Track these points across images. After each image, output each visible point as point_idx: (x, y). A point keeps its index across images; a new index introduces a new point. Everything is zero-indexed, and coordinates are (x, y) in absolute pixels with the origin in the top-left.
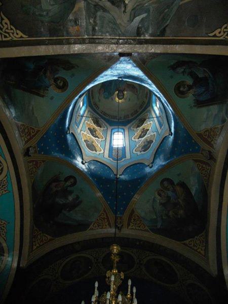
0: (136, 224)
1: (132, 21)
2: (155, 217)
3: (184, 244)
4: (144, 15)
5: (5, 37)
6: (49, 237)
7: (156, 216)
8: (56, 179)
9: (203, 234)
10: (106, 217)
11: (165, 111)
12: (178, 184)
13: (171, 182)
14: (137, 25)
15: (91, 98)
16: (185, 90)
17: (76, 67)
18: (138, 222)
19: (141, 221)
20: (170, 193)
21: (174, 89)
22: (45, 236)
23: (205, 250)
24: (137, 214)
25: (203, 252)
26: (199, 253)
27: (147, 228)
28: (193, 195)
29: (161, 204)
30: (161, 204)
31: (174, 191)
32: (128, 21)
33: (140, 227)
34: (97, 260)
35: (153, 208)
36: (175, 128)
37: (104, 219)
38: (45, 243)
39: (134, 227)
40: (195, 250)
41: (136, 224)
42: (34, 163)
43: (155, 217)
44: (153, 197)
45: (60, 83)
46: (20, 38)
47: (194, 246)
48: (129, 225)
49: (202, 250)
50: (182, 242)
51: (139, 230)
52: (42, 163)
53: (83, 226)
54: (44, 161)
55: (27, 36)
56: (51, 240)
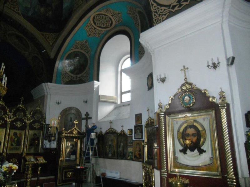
3: (43, 35)
4: (23, 115)
5: (155, 20)
7: (31, 6)
9: (57, 34)
11: (107, 102)
23: (53, 43)
25: (51, 44)
26: (49, 43)
27: (19, 12)
28: (64, 7)
33: (14, 8)
36: (219, 145)
39: (9, 6)
40: (47, 40)
41: (12, 5)
45: (54, 122)
46: (164, 11)
47: (48, 38)
55: (167, 8)
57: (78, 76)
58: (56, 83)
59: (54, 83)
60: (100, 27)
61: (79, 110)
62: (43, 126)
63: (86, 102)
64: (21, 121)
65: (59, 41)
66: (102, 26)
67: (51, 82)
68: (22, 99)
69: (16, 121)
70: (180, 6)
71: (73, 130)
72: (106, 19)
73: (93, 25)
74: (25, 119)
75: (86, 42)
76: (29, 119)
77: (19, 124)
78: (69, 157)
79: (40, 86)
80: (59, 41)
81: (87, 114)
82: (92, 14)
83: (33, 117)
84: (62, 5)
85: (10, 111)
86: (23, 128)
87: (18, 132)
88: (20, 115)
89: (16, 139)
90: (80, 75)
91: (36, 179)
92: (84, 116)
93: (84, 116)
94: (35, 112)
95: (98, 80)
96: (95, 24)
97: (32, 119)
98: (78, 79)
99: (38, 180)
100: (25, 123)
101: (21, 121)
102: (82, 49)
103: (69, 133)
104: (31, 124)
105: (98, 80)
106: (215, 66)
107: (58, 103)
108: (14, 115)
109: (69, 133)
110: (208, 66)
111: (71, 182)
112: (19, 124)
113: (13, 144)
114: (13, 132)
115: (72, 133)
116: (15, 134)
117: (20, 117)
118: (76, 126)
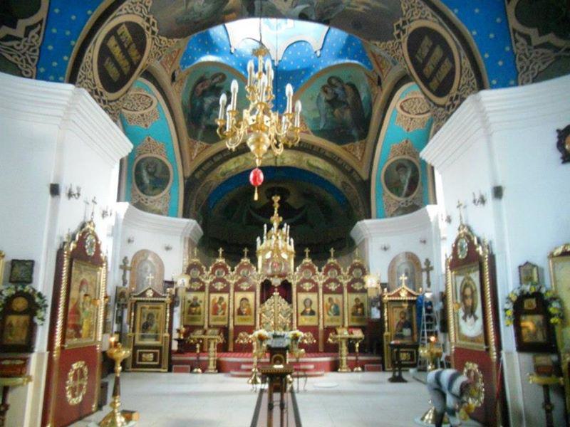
3: (346, 149)
26: (357, 158)
27: (308, 129)
50: (343, 146)
56: (207, 147)
57: (409, 199)
58: (377, 217)
59: (374, 219)
60: (420, 114)
61: (415, 255)
62: (115, 327)
63: (425, 242)
64: (336, 281)
65: (368, 152)
66: (421, 112)
67: (369, 216)
68: (332, 251)
69: (329, 281)
70: (454, 105)
71: (400, 290)
72: (415, 109)
73: (406, 114)
74: (340, 278)
75: (407, 142)
76: (345, 278)
77: (333, 287)
78: (401, 331)
79: (355, 227)
80: (368, 152)
81: (428, 262)
82: (396, 103)
83: (350, 273)
84: (359, 97)
85: (320, 270)
86: (340, 291)
87: (334, 297)
88: (332, 274)
89: (332, 307)
90: (413, 196)
91: (353, 358)
92: (424, 266)
93: (424, 266)
94: (354, 267)
95: (435, 202)
96: (408, 112)
97: (349, 277)
98: (409, 204)
99: (357, 360)
100: (341, 284)
101: (336, 281)
102: (404, 154)
103: (394, 295)
104: (349, 284)
105: (435, 202)
106: (483, 201)
107: (385, 249)
108: (325, 274)
109: (394, 295)
110: (474, 201)
111: (407, 369)
112: (333, 287)
113: (330, 313)
114: (327, 297)
115: (398, 294)
116: (330, 300)
117: (333, 277)
118: (403, 284)
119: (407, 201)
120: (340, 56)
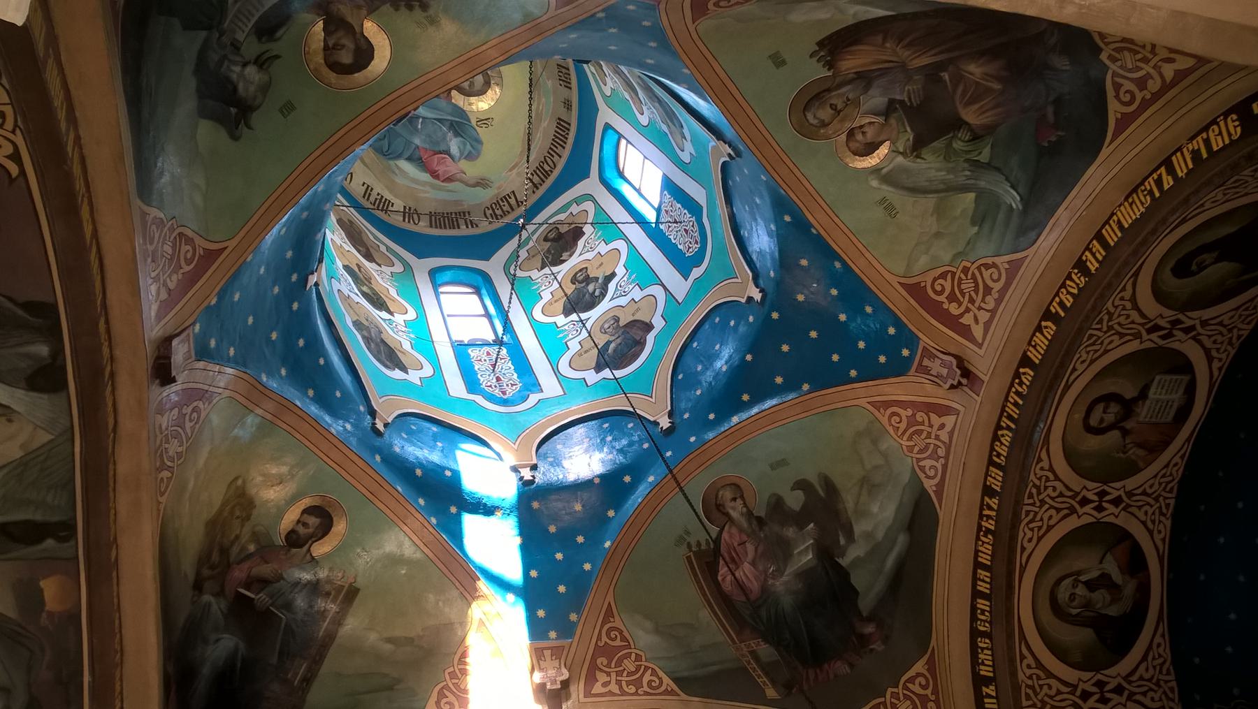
0: (972, 301)
1: (8, 407)
2: (972, 196)
3: (1124, 122)
6: (920, 666)
8: (707, 561)
10: (909, 412)
12: (830, 65)
13: (812, 97)
14: (20, 393)
15: (464, 231)
16: (351, 46)
17: (240, 482)
18: (968, 286)
19: (965, 270)
20: (876, 99)
21: (372, 58)
22: (911, 680)
24: (929, 279)
26: (951, 434)
29: (917, 147)
30: (917, 147)
31: (864, 79)
32: (10, 421)
34: (1085, 502)
35: (925, 191)
37: (912, 421)
38: (935, 692)
41: (972, 301)
42: (602, 661)
43: (972, 196)
44: (875, 183)
48: (965, 332)
49: (942, 426)
51: (999, 301)
52: (617, 623)
53: (920, 516)
54: (609, 614)
119: (1102, 494)
120: (1029, 223)
